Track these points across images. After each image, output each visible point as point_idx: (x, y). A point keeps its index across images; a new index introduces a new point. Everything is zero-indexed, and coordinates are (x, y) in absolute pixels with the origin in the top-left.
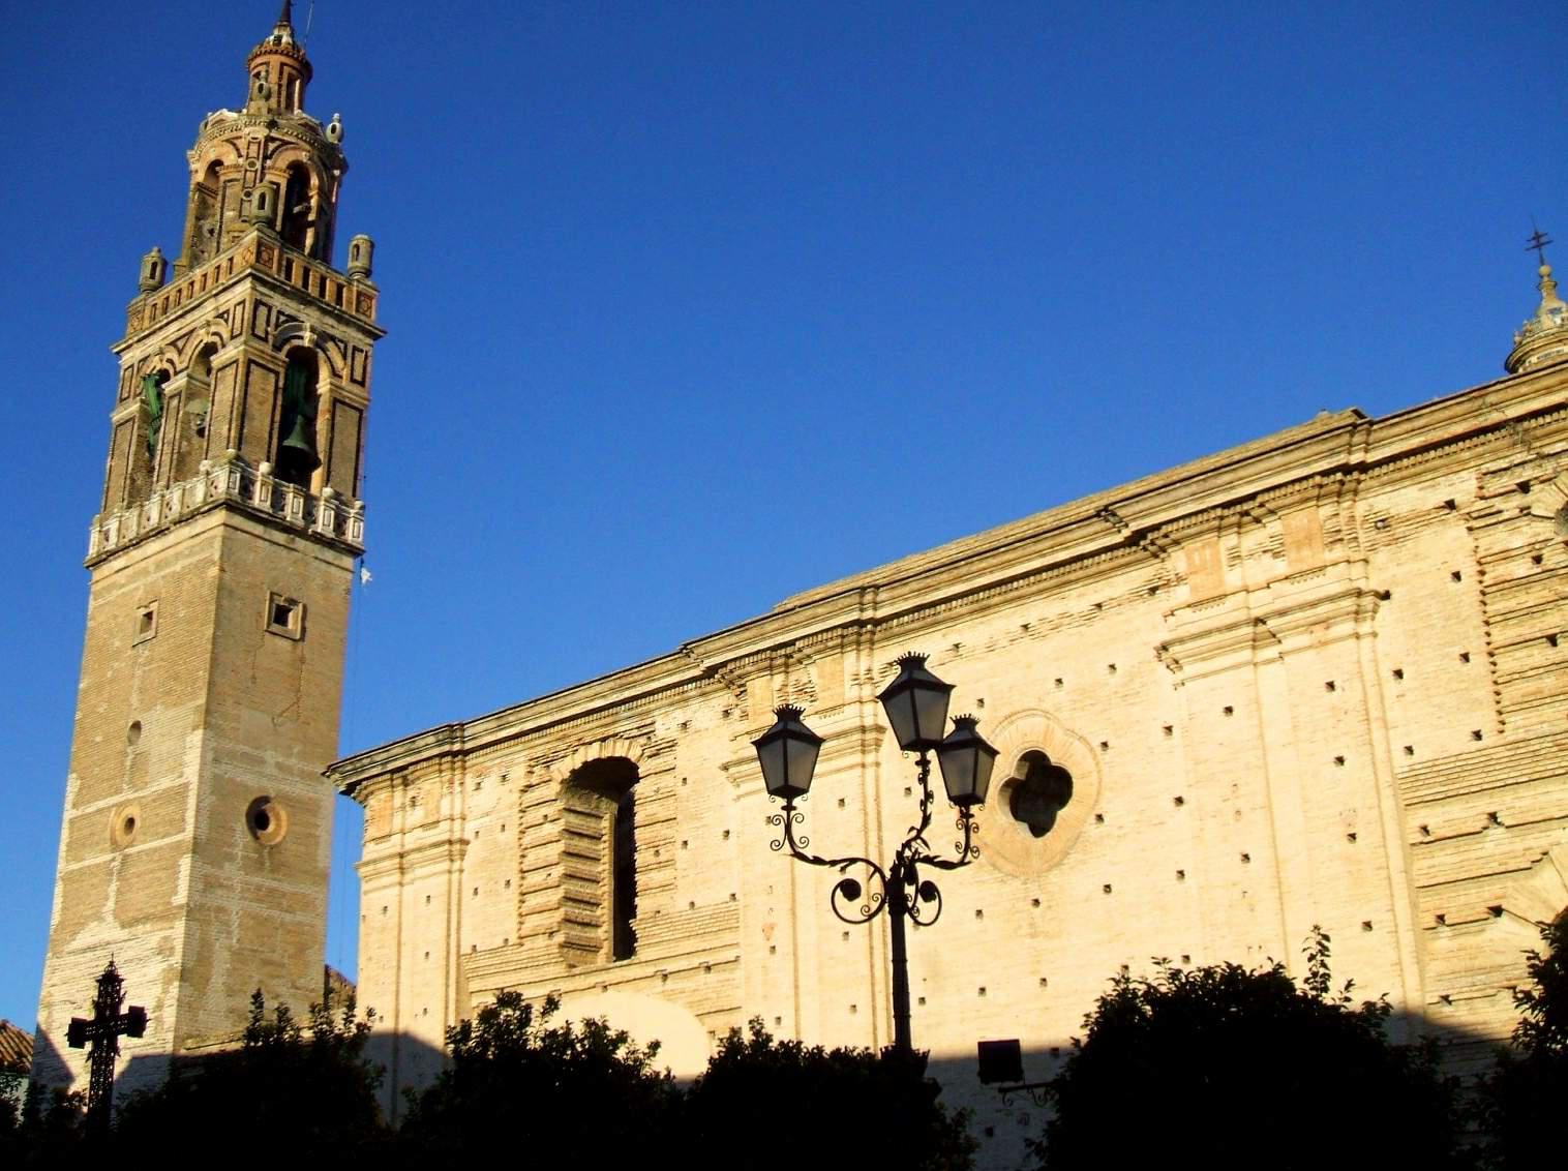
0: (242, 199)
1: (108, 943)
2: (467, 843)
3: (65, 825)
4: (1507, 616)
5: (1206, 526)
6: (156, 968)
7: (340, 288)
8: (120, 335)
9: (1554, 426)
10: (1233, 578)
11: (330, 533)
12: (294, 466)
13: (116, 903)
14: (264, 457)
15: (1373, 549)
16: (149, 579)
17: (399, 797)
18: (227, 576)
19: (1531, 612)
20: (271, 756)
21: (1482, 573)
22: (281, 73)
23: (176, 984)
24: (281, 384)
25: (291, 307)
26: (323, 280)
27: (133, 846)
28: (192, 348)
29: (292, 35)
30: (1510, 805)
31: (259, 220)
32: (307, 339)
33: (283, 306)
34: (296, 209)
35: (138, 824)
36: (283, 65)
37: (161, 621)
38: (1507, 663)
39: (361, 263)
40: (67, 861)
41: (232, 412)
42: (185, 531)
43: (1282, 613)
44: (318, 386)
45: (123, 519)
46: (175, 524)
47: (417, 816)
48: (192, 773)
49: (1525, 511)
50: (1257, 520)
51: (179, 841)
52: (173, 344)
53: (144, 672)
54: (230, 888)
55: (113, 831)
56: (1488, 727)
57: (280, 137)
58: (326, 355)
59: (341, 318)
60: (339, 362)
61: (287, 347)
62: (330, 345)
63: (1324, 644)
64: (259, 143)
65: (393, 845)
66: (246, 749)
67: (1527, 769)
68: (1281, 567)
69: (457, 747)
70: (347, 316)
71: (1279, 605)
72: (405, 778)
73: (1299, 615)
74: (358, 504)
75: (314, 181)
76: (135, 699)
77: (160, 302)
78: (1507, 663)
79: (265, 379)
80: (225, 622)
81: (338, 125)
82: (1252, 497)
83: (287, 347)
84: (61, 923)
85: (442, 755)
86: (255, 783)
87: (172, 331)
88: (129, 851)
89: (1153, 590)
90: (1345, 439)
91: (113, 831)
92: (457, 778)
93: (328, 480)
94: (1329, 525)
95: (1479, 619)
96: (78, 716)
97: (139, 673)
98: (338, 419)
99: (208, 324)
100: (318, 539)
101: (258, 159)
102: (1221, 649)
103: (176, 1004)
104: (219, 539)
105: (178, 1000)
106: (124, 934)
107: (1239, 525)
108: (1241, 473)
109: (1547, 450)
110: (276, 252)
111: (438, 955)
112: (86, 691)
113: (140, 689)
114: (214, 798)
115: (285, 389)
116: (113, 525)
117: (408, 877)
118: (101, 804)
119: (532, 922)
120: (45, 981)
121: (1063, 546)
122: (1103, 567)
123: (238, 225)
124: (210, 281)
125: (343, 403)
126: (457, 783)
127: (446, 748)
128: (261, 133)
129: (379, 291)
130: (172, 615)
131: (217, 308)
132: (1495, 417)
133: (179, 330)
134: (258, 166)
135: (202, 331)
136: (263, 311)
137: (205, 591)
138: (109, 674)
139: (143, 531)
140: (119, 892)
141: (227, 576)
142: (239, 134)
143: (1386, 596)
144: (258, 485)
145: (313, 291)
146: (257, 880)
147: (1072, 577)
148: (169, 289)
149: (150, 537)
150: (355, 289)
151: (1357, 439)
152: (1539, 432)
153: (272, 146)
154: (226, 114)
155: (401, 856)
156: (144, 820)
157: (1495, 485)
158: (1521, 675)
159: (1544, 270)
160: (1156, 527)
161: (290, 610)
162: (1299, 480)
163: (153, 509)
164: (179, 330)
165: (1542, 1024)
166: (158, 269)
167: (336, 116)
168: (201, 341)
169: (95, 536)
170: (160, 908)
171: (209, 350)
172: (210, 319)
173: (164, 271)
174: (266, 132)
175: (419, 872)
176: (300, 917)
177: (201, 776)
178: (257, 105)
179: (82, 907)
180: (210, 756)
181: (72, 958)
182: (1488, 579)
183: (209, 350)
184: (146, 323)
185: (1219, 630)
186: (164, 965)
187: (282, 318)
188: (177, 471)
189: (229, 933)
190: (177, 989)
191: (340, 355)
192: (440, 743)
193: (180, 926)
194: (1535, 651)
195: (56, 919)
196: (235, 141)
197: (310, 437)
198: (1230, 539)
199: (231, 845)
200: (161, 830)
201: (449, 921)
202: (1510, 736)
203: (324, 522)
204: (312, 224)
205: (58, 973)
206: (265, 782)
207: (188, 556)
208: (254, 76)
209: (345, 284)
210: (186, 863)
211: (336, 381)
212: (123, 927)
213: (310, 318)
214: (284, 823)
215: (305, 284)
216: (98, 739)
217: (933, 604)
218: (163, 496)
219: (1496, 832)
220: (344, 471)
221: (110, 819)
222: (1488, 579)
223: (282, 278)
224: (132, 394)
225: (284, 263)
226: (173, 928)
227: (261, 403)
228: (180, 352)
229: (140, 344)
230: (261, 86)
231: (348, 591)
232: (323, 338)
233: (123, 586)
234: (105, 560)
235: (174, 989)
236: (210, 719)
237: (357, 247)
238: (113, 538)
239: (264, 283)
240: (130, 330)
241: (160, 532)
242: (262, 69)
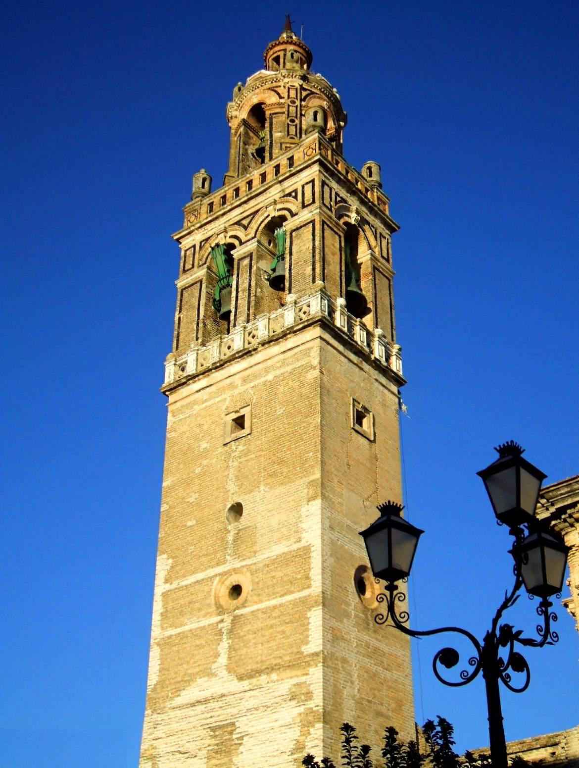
0: (288, 124)
1: (223, 696)
6: (291, 712)
8: (180, 226)
13: (230, 658)
14: (339, 295)
16: (236, 392)
23: (320, 725)
27: (245, 607)
32: (353, 218)
33: (338, 191)
37: (254, 421)
40: (163, 628)
41: (314, 256)
42: (275, 349)
44: (358, 257)
45: (199, 352)
46: (263, 345)
51: (305, 597)
52: (238, 223)
53: (240, 463)
54: (349, 642)
55: (217, 598)
57: (309, 88)
58: (365, 234)
60: (373, 243)
62: (366, 227)
64: (297, 89)
70: (376, 209)
76: (232, 487)
79: (334, 239)
80: (327, 415)
84: (161, 683)
87: (235, 215)
88: (238, 612)
91: (217, 598)
93: (377, 324)
99: (275, 202)
101: (297, 99)
103: (321, 744)
105: (324, 741)
106: (236, 685)
112: (169, 488)
113: (236, 476)
118: (200, 576)
120: (144, 735)
128: (297, 82)
129: (389, 200)
131: (283, 191)
133: (241, 213)
137: (305, 391)
138: (198, 470)
140: (231, 648)
141: (325, 378)
142: (279, 84)
149: (236, 358)
150: (375, 194)
153: (304, 94)
161: (365, 416)
164: (241, 213)
168: (269, 215)
170: (288, 658)
172: (277, 199)
177: (323, 539)
179: (185, 666)
181: (178, 713)
186: (302, 709)
188: (256, 309)
189: (352, 682)
190: (322, 730)
191: (373, 236)
193: (315, 676)
195: (153, 678)
196: (276, 89)
200: (279, 590)
205: (160, 727)
208: (274, 59)
209: (370, 189)
210: (316, 617)
212: (241, 678)
216: (189, 523)
218: (245, 328)
221: (214, 587)
224: (196, 264)
226: (307, 674)
229: (201, 230)
233: (206, 401)
234: (184, 383)
241: (246, 353)
242: (281, 54)
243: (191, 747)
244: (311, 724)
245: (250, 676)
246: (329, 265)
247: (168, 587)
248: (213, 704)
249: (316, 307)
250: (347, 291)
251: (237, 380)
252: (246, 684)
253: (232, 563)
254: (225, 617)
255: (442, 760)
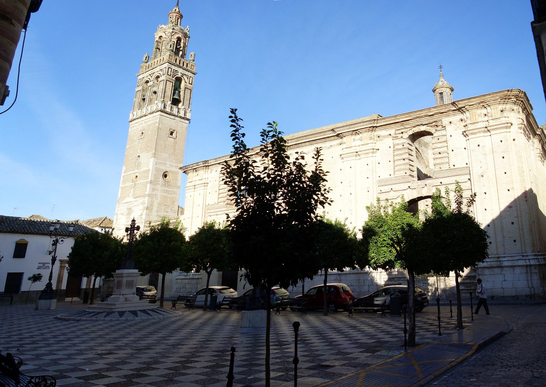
2: (208, 183)
3: (122, 177)
4: (397, 155)
5: (349, 134)
6: (141, 207)
7: (187, 64)
9: (407, 123)
10: (353, 144)
11: (183, 116)
12: (175, 102)
15: (377, 141)
16: (143, 125)
17: (195, 174)
18: (160, 126)
19: (401, 154)
20: (168, 163)
21: (394, 147)
22: (176, 17)
23: (146, 210)
24: (173, 85)
25: (176, 68)
26: (184, 62)
28: (154, 76)
29: (179, 9)
30: (395, 187)
31: (170, 50)
34: (178, 47)
35: (138, 177)
36: (176, 15)
38: (397, 163)
39: (192, 58)
43: (361, 151)
47: (198, 178)
48: (151, 167)
49: (402, 137)
50: (358, 134)
52: (150, 75)
55: (133, 178)
56: (392, 174)
59: (187, 70)
61: (175, 77)
63: (367, 157)
65: (193, 184)
66: (163, 162)
67: (404, 181)
68: (361, 143)
69: (207, 165)
71: (360, 150)
72: (196, 170)
73: (364, 152)
74: (190, 109)
75: (182, 41)
76: (139, 151)
77: (147, 66)
78: (397, 163)
81: (188, 29)
82: (357, 130)
83: (175, 77)
85: (204, 166)
86: (164, 168)
87: (150, 72)
88: (136, 183)
89: (341, 144)
90: (373, 121)
91: (133, 178)
92: (207, 171)
94: (370, 136)
95: (392, 155)
96: (126, 154)
97: (140, 145)
98: (186, 92)
99: (158, 71)
100: (181, 117)
102: (351, 156)
104: (159, 118)
107: (355, 134)
108: (356, 126)
109: (406, 127)
110: (173, 57)
111: (201, 205)
114: (155, 172)
115: (174, 86)
116: (135, 113)
117: (196, 190)
118: (130, 173)
119: (220, 200)
121: (326, 135)
122: (332, 139)
123: (165, 50)
124: (158, 62)
125: (187, 88)
126: (207, 171)
127: (205, 165)
128: (171, 31)
130: (148, 133)
132: (397, 121)
134: (170, 38)
135: (157, 73)
136: (170, 69)
139: (142, 115)
141: (160, 126)
143: (378, 150)
144: (167, 106)
145: (181, 65)
146: (164, 188)
147: (327, 140)
148: (149, 63)
151: (375, 122)
152: (405, 124)
153: (173, 34)
154: (163, 26)
155: (195, 186)
156: (140, 176)
157: (398, 132)
158: (398, 165)
159: (441, 73)
160: (341, 133)
162: (365, 128)
163: (144, 110)
165: (148, 235)
166: (147, 58)
167: (188, 26)
169: (131, 115)
171: (158, 77)
173: (148, 59)
174: (172, 30)
175: (198, 189)
176: (173, 196)
177: (153, 168)
178: (170, 25)
180: (155, 163)
182: (395, 148)
183: (158, 77)
184: (144, 70)
185: (350, 153)
186: (143, 206)
187: (174, 71)
192: (204, 164)
193: (147, 198)
194: (401, 161)
195: (119, 196)
197: (179, 96)
198: (353, 137)
199: (159, 181)
201: (204, 199)
202: (396, 175)
203: (182, 114)
204: (181, 50)
206: (167, 168)
207: (152, 121)
211: (186, 84)
212: (134, 198)
213: (180, 71)
214: (171, 177)
215: (180, 64)
216: (130, 159)
217: (299, 144)
219: (392, 192)
220: (187, 102)
222: (395, 148)
223: (174, 62)
225: (175, 59)
227: (169, 89)
228: (151, 77)
230: (171, 21)
231: (187, 128)
232: (183, 75)
235: (145, 211)
236: (155, 155)
237: (191, 55)
238: (135, 115)
239: (170, 64)
240: (140, 71)
243: (124, 213)
244: (144, 210)
245: (136, 198)
246: (167, 92)
247: (124, 174)
248: (129, 204)
249: (160, 106)
250: (173, 98)
251: (143, 122)
252: (135, 200)
253: (136, 171)
254: (133, 183)
255: (268, 212)
